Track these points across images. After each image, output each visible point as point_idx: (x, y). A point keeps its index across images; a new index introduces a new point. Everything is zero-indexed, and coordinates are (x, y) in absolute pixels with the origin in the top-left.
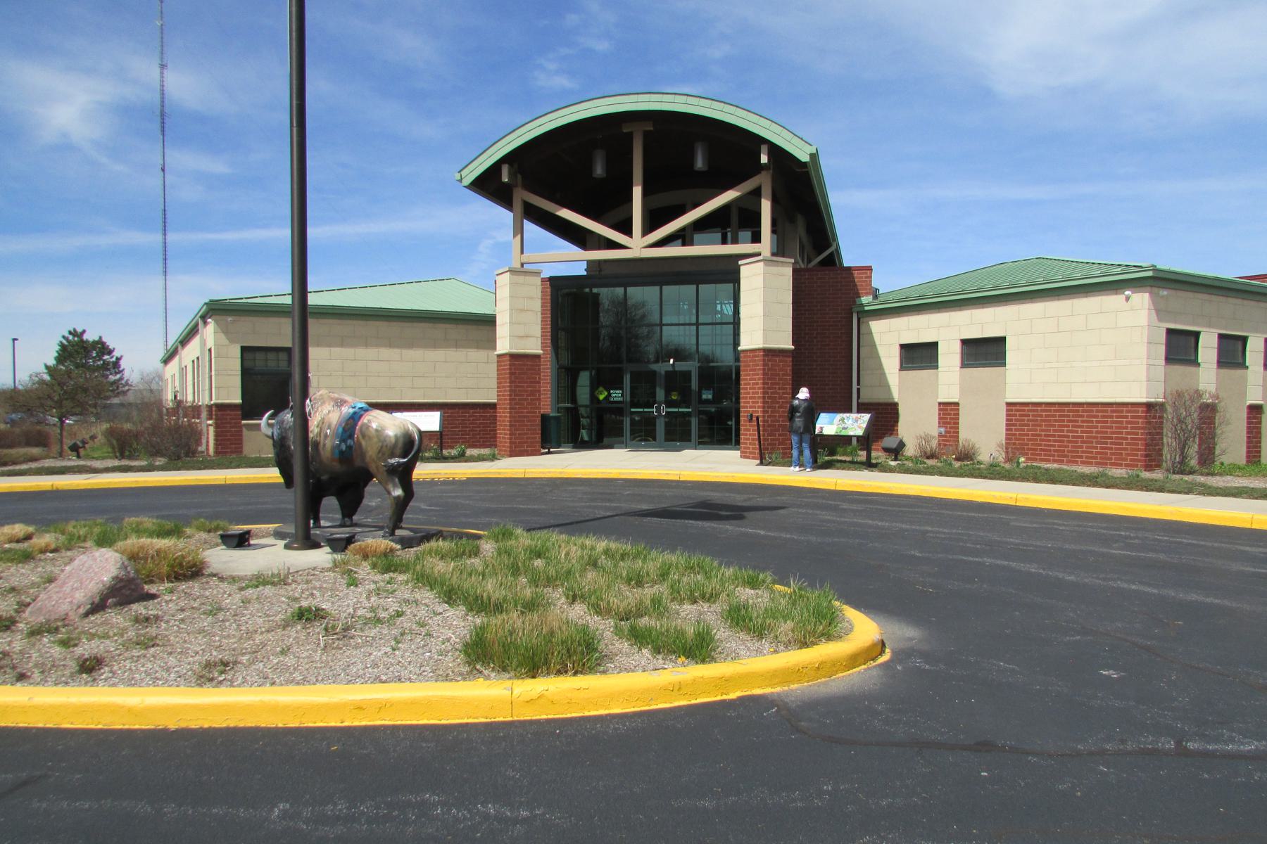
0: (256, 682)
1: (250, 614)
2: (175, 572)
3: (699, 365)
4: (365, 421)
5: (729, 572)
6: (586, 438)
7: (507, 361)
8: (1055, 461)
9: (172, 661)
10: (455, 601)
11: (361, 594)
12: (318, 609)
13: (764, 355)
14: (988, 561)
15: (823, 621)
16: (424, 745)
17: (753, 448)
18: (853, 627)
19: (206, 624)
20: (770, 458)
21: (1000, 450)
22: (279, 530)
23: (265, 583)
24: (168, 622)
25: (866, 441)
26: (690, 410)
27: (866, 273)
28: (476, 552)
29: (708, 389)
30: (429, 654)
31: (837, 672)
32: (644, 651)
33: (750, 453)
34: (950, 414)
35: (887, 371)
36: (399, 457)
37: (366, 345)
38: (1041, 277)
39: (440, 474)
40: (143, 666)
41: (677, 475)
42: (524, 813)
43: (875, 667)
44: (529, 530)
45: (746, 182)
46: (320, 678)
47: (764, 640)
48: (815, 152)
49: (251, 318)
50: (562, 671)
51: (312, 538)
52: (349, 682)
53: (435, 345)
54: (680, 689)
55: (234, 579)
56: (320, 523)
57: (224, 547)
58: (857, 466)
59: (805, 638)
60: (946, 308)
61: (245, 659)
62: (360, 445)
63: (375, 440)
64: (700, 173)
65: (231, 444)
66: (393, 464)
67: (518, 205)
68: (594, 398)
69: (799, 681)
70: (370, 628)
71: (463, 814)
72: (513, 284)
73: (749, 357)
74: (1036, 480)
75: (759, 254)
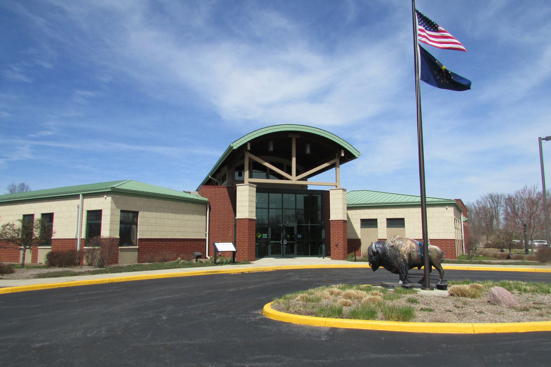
3: (297, 224)
29: (300, 234)
37: (164, 212)
39: (260, 269)
41: (345, 266)
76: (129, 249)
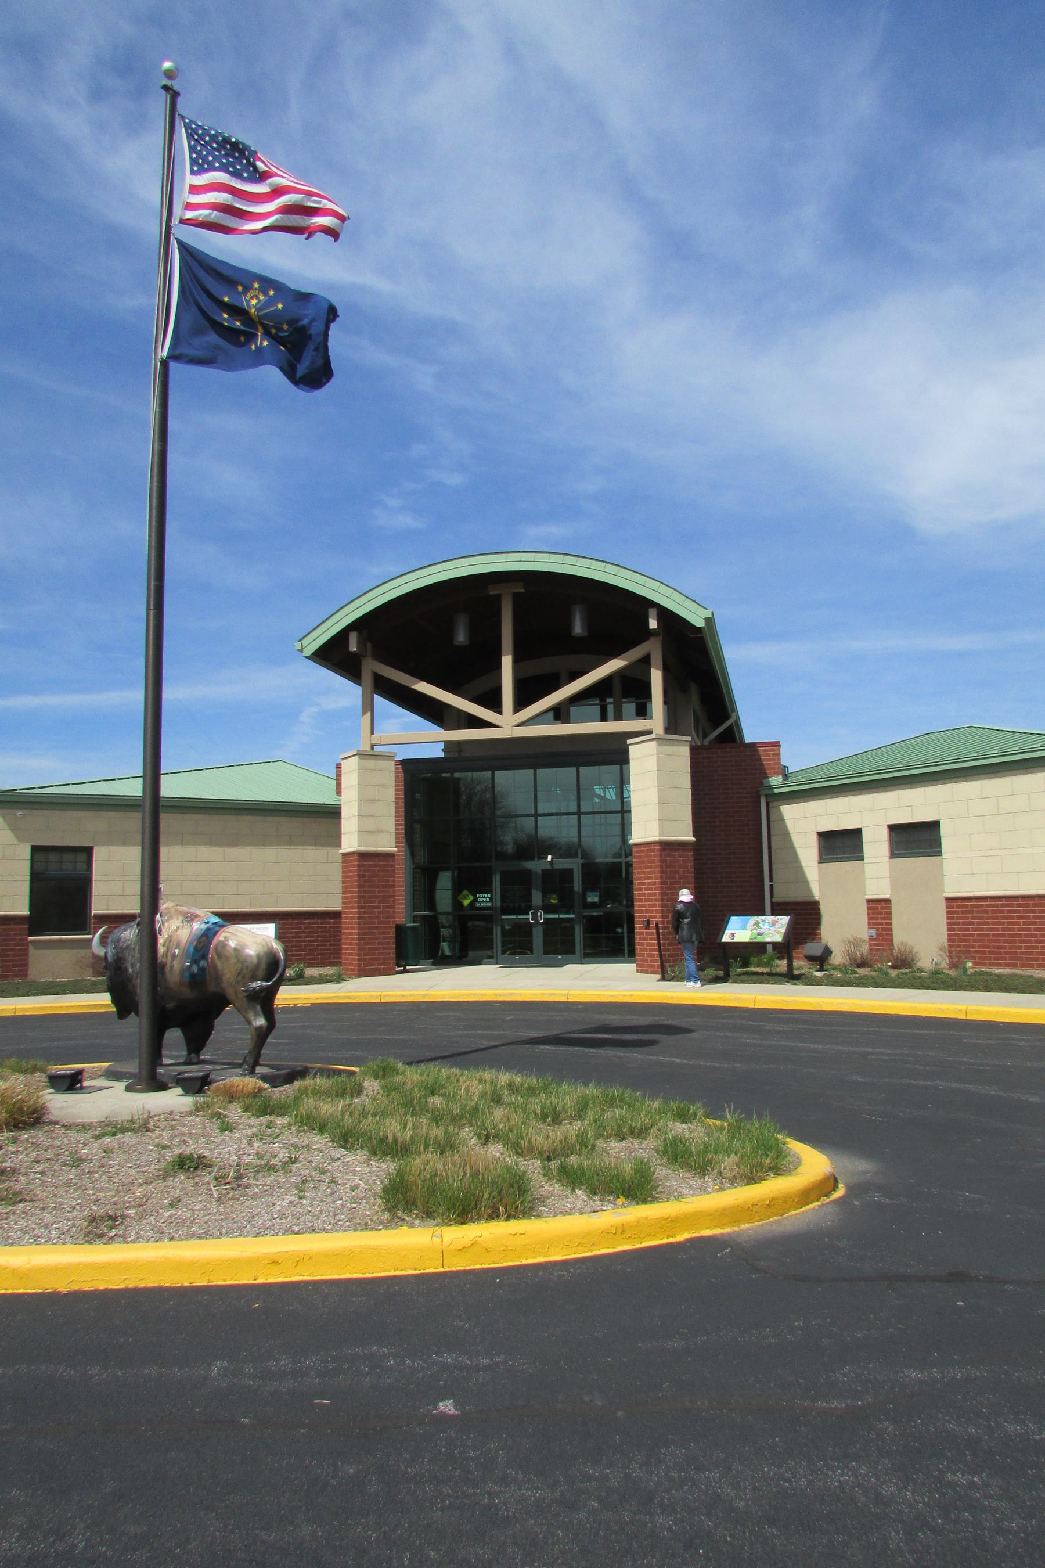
0: (152, 1237)
1: (119, 1165)
2: (14, 1119)
3: (582, 861)
4: (221, 938)
5: (656, 1104)
6: (447, 952)
7: (355, 861)
8: (1007, 965)
9: (48, 1217)
10: (352, 1145)
11: (240, 1139)
12: (201, 1157)
13: (660, 850)
14: (941, 1084)
15: (769, 1153)
16: (354, 1299)
17: (652, 961)
18: (800, 1160)
19: (72, 1176)
20: (673, 972)
21: (943, 954)
22: (114, 1069)
23: (123, 1130)
24: (26, 1174)
25: (784, 949)
26: (572, 916)
27: (774, 750)
28: (359, 1090)
29: (593, 890)
30: (341, 1202)
31: (789, 1210)
32: (579, 1192)
33: (648, 966)
34: (881, 913)
35: (804, 864)
36: (262, 980)
38: (973, 752)
40: (16, 1224)
41: (565, 995)
42: (485, 1361)
43: (830, 1203)
44: (410, 1064)
46: (224, 1231)
47: (707, 1177)
48: (710, 616)
49: (46, 812)
50: (494, 1216)
51: (158, 1077)
52: (258, 1235)
54: (623, 1232)
55: (84, 1127)
56: (162, 1061)
57: (52, 1090)
58: (776, 978)
59: (752, 1173)
61: (132, 1212)
62: (215, 966)
63: (234, 960)
64: (579, 639)
65: (14, 966)
66: (254, 989)
67: (367, 677)
68: (457, 904)
69: (750, 1221)
70: (264, 1176)
71: (419, 1364)
72: (362, 770)
73: (643, 851)
74: (988, 989)
75: (650, 732)
76: (61, 941)
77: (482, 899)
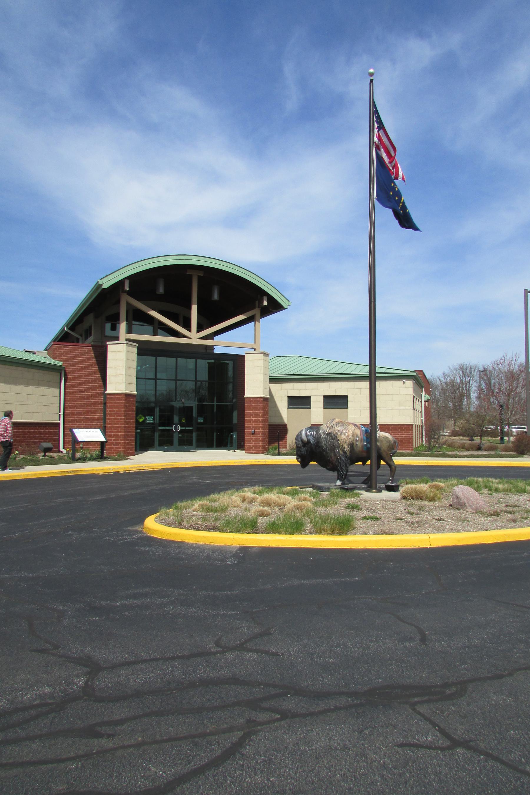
3: (197, 403)
29: (201, 416)
41: (264, 462)
45: (249, 312)
53: (28, 383)
60: (292, 381)
63: (385, 442)
77: (149, 419)
